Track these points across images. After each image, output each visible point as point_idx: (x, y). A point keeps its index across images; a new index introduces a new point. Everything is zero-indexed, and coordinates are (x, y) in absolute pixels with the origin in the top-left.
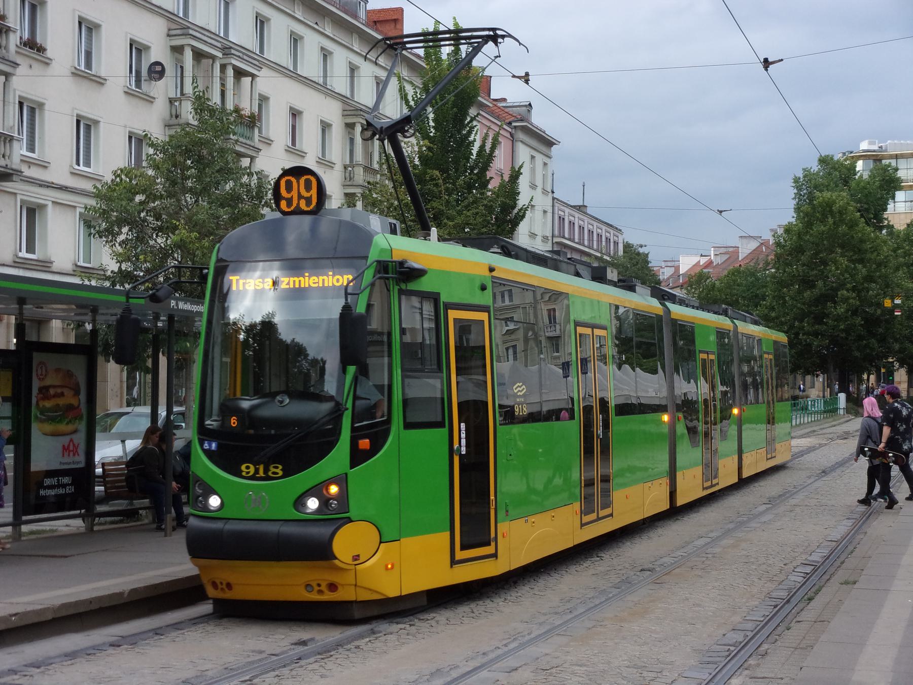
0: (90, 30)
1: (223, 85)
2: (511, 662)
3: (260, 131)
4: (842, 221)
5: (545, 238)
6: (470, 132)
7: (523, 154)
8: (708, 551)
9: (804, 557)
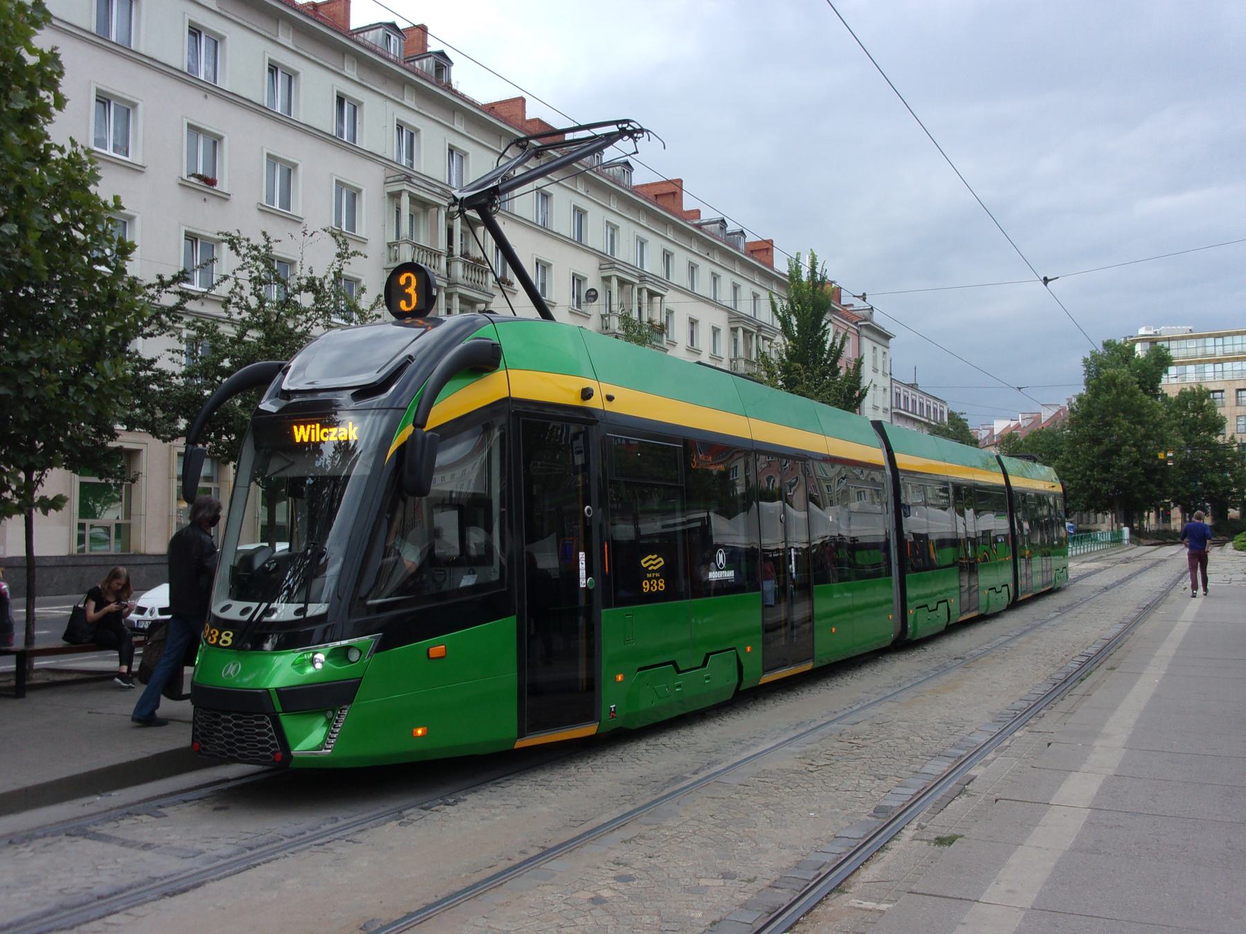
0: (544, 268)
1: (640, 303)
2: (854, 718)
4: (1124, 392)
5: (885, 410)
6: (824, 334)
7: (867, 345)
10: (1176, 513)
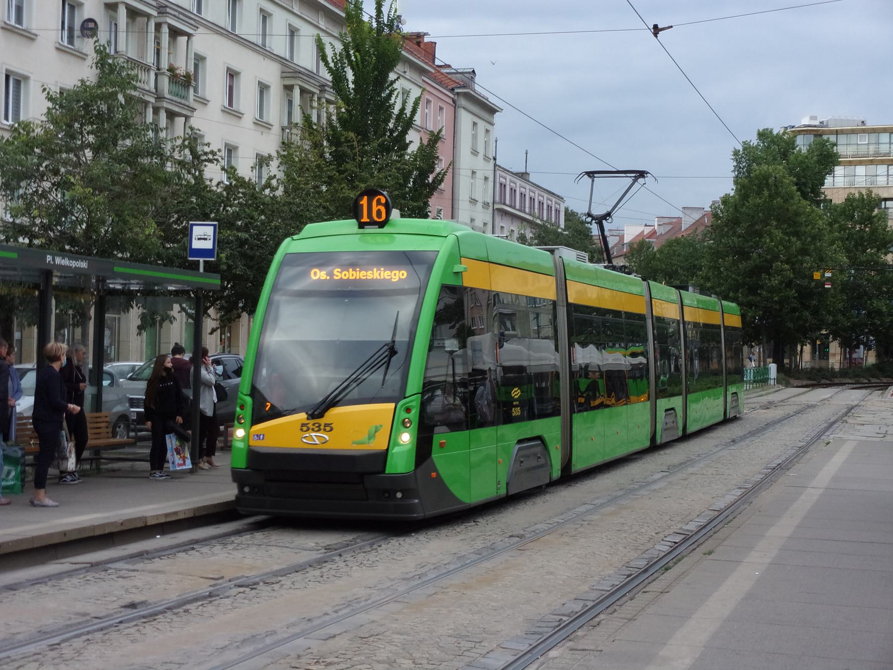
3: (196, 91)
4: (777, 194)
6: (390, 95)
8: (585, 518)
9: (679, 526)
10: (834, 347)
